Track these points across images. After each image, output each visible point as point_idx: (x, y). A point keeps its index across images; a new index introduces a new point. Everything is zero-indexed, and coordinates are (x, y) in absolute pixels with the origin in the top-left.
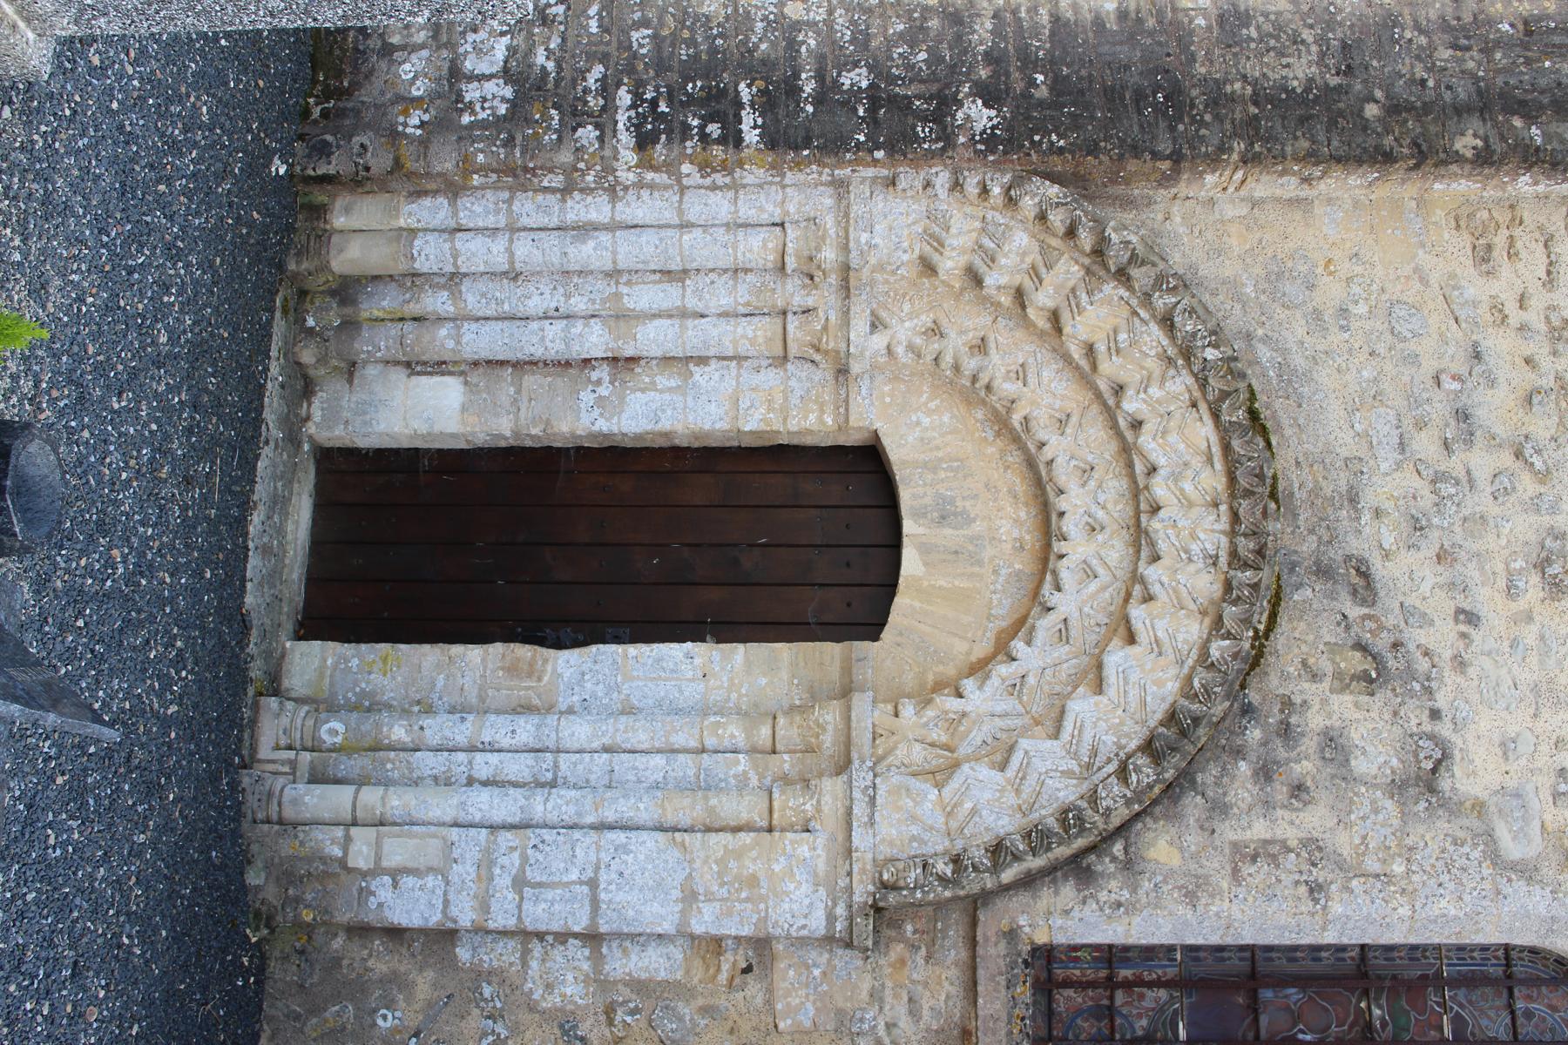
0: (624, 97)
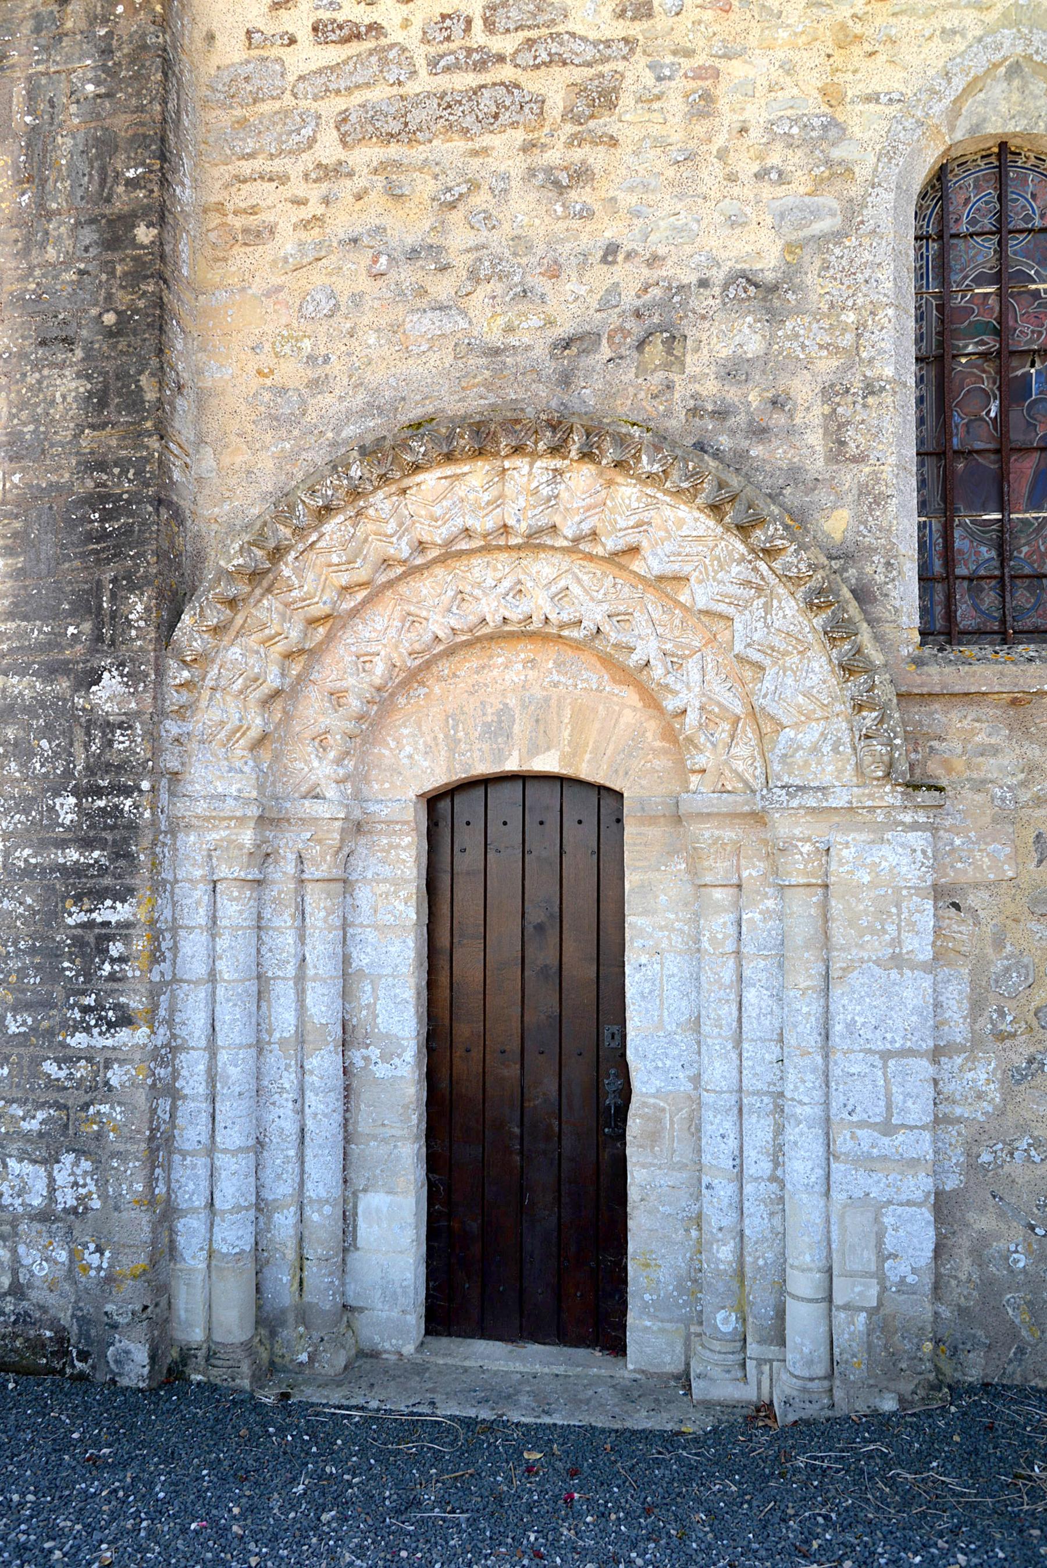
0: (79, 1040)
